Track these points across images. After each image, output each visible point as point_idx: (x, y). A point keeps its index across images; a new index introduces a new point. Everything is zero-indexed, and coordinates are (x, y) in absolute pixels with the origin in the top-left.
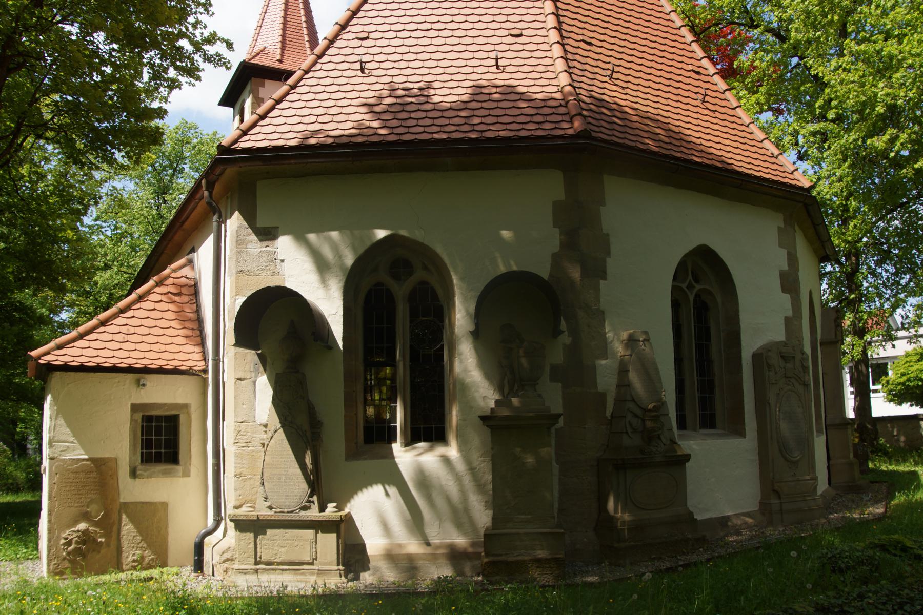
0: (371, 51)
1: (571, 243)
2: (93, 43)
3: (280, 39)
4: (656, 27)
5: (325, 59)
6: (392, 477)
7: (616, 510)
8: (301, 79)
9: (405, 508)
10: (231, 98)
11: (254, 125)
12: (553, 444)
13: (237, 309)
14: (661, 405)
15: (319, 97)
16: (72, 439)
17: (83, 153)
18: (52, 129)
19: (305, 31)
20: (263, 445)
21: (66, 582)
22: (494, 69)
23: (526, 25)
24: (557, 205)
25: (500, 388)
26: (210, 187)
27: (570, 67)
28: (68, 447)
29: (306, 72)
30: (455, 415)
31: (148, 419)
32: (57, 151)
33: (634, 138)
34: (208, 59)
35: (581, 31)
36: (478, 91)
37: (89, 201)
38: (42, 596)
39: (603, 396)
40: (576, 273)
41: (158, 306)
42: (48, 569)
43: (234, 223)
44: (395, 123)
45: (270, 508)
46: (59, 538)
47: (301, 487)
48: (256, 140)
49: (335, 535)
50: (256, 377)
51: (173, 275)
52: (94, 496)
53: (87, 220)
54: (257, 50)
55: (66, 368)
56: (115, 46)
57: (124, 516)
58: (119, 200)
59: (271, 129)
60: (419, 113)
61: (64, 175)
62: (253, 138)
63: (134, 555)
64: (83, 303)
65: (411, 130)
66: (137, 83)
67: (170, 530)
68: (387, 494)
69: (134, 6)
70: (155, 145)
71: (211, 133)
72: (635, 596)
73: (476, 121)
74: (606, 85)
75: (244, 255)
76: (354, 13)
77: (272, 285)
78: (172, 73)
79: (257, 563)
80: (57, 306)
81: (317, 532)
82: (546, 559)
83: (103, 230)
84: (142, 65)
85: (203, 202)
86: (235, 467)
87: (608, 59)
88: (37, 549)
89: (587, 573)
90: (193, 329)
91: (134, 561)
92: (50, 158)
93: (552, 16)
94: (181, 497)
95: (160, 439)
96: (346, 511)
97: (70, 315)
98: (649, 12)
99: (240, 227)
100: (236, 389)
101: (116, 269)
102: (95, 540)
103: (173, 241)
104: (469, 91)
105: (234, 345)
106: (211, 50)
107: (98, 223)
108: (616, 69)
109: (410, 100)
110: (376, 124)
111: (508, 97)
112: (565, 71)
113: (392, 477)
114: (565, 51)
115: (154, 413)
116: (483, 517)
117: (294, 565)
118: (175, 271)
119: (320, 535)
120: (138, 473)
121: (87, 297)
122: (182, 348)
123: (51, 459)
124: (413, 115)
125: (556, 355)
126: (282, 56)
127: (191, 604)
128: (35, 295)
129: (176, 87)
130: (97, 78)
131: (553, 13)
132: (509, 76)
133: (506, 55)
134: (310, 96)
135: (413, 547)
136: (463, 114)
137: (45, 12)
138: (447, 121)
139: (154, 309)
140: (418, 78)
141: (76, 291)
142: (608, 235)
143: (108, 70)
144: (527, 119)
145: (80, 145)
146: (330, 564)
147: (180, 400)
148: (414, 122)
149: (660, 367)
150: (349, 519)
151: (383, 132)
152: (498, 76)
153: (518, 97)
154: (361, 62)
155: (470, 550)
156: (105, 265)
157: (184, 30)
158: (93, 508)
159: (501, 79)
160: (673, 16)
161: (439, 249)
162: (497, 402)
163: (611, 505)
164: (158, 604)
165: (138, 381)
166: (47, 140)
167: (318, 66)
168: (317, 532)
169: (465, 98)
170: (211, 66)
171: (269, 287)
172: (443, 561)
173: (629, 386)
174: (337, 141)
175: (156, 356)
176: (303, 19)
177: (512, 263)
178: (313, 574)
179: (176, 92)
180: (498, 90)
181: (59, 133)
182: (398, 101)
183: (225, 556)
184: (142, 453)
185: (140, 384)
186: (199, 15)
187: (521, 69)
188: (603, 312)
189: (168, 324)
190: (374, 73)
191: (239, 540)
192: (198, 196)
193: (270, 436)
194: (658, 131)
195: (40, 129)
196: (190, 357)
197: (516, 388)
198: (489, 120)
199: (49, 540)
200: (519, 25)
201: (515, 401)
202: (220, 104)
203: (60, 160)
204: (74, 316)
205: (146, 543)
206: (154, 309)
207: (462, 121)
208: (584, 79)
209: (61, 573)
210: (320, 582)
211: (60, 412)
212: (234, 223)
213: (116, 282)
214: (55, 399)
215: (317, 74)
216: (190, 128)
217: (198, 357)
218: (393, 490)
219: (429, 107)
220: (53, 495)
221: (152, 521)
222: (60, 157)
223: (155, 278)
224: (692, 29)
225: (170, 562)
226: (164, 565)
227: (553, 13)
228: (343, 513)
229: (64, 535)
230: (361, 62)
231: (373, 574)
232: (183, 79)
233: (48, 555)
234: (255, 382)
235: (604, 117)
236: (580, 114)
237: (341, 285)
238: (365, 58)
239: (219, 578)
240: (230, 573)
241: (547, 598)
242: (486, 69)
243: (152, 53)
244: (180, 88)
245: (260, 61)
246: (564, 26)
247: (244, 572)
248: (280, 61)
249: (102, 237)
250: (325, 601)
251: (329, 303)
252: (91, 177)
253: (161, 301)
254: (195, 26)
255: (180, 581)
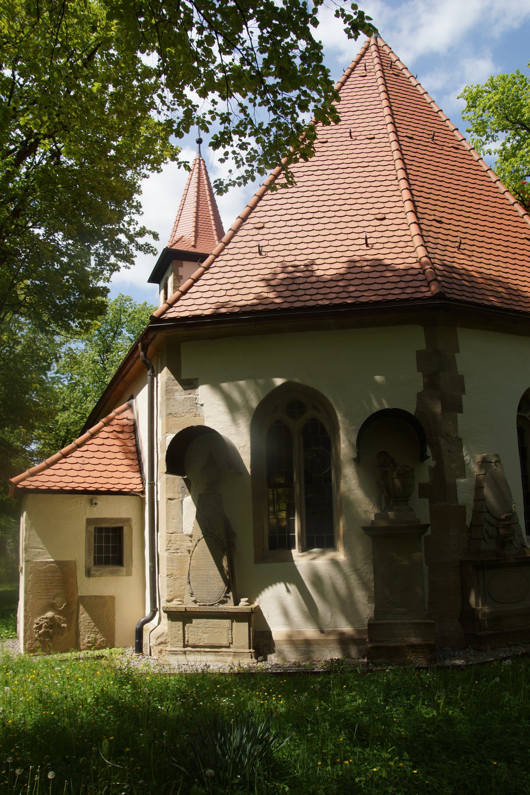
0: (266, 237)
1: (432, 383)
2: (54, 240)
3: (194, 229)
4: (494, 205)
5: (231, 245)
6: (292, 576)
7: (477, 604)
8: (213, 262)
9: (303, 602)
10: (157, 276)
11: (177, 299)
12: (423, 549)
13: (168, 444)
14: (512, 515)
15: (227, 275)
16: (42, 546)
17: (47, 324)
18: (25, 307)
19: (213, 222)
20: (189, 551)
21: (38, 658)
22: (364, 247)
23: (388, 210)
24: (420, 355)
25: (378, 504)
26: (145, 348)
27: (425, 242)
28: (39, 552)
29: (217, 256)
30: (341, 526)
31: (99, 530)
32: (28, 321)
33: (481, 297)
34: (139, 248)
35: (432, 213)
36: (352, 264)
37: (51, 359)
38: (21, 670)
39: (463, 508)
40: (438, 409)
41: (107, 442)
42: (25, 647)
43: (164, 376)
44: (287, 293)
45: (195, 602)
46: (32, 624)
47: (219, 585)
48: (181, 311)
49: (247, 624)
50: (183, 497)
51: (117, 417)
52: (59, 591)
53: (50, 374)
54: (176, 239)
55: (37, 491)
56: (71, 242)
57: (81, 607)
58: (75, 358)
59: (190, 302)
60: (306, 284)
61: (34, 340)
62: (177, 309)
63: (89, 637)
64: (47, 437)
65: (301, 298)
66: (86, 268)
67: (117, 618)
68: (288, 591)
69: (84, 211)
70: (101, 315)
71: (142, 303)
72: (498, 679)
73: (352, 289)
74: (455, 255)
75: (172, 401)
76: (252, 208)
77: (195, 424)
78: (113, 260)
79: (185, 646)
80: (28, 440)
81: (232, 622)
82: (420, 645)
83: (62, 380)
84: (90, 254)
85: (139, 361)
86: (168, 569)
87: (456, 234)
88: (15, 630)
89: (455, 657)
90: (133, 459)
91: (89, 642)
92: (24, 328)
93: (408, 202)
94: (127, 594)
95: (110, 546)
96: (256, 604)
97: (38, 446)
98: (487, 193)
99: (169, 379)
100: (168, 507)
101: (72, 411)
102: (59, 625)
103: (116, 392)
104: (345, 265)
105: (166, 473)
106: (141, 241)
107: (58, 375)
108: (463, 241)
109: (298, 274)
110: (271, 295)
111: (376, 269)
112: (422, 245)
113: (292, 576)
114: (421, 229)
115: (104, 525)
116: (366, 610)
117: (214, 648)
118: (118, 414)
119: (235, 624)
120: (92, 572)
121: (50, 433)
122: (125, 475)
123: (27, 561)
124: (301, 286)
125: (423, 475)
126: (196, 241)
127: (134, 680)
128: (12, 432)
129: (116, 270)
130: (57, 266)
131: (409, 200)
132: (376, 252)
133: (373, 235)
134: (220, 275)
135: (310, 632)
136: (341, 284)
137: (20, 222)
138: (328, 290)
139: (103, 444)
140: (305, 257)
141: (42, 427)
142: (462, 376)
143: (65, 260)
144: (393, 286)
145: (45, 318)
146: (243, 647)
147: (124, 515)
148: (302, 292)
149: (510, 483)
150: (258, 611)
151: (278, 301)
152: (369, 252)
153: (384, 268)
154: (259, 247)
155: (357, 637)
156: (64, 407)
157: (122, 227)
158: (57, 600)
159: (370, 254)
160: (507, 195)
161: (326, 394)
162: (376, 515)
163: (472, 599)
164: (108, 678)
165: (91, 500)
166: (21, 314)
167: (226, 251)
168: (232, 622)
169: (342, 271)
170: (142, 253)
171: (192, 427)
172: (335, 646)
173: (484, 500)
174: (243, 309)
175: (105, 481)
176: (211, 213)
177: (384, 402)
178: (229, 656)
179: (115, 274)
180: (368, 263)
181: (29, 309)
182: (289, 276)
183: (160, 640)
184: (95, 557)
185: (93, 503)
186: (132, 215)
187: (385, 245)
188: (461, 440)
189: (113, 455)
190: (270, 254)
191: (170, 628)
192: (136, 356)
193: (194, 544)
194: (500, 289)
195: (16, 306)
196: (131, 481)
197: (391, 503)
198: (362, 288)
199: (25, 625)
200: (382, 211)
201: (391, 514)
202: (149, 281)
203: (30, 329)
204: (41, 447)
205: (98, 628)
206: (103, 444)
207: (341, 289)
208: (437, 251)
209: (34, 651)
210: (236, 663)
211: (31, 526)
212: (164, 376)
213: (72, 420)
214: (29, 514)
215: (225, 258)
216: (126, 300)
217: (138, 481)
218: (292, 588)
219: (313, 279)
220: (28, 589)
221: (103, 610)
222: (30, 326)
223: (104, 420)
224: (522, 202)
225: (116, 644)
226: (112, 646)
227: (409, 200)
228: (253, 606)
229: (36, 621)
230: (259, 247)
231: (278, 656)
232: (121, 264)
233: (25, 637)
234: (182, 501)
235: (455, 281)
236: (435, 280)
237: (249, 422)
238: (262, 243)
239: (155, 657)
240: (164, 654)
241: (422, 679)
242: (358, 247)
243: (98, 246)
244: (119, 271)
245: (179, 247)
246: (419, 210)
247: (174, 653)
248: (194, 246)
249: (61, 386)
250: (240, 678)
251: (239, 437)
252: (52, 341)
253: (108, 438)
254: (129, 223)
255: (125, 659)
